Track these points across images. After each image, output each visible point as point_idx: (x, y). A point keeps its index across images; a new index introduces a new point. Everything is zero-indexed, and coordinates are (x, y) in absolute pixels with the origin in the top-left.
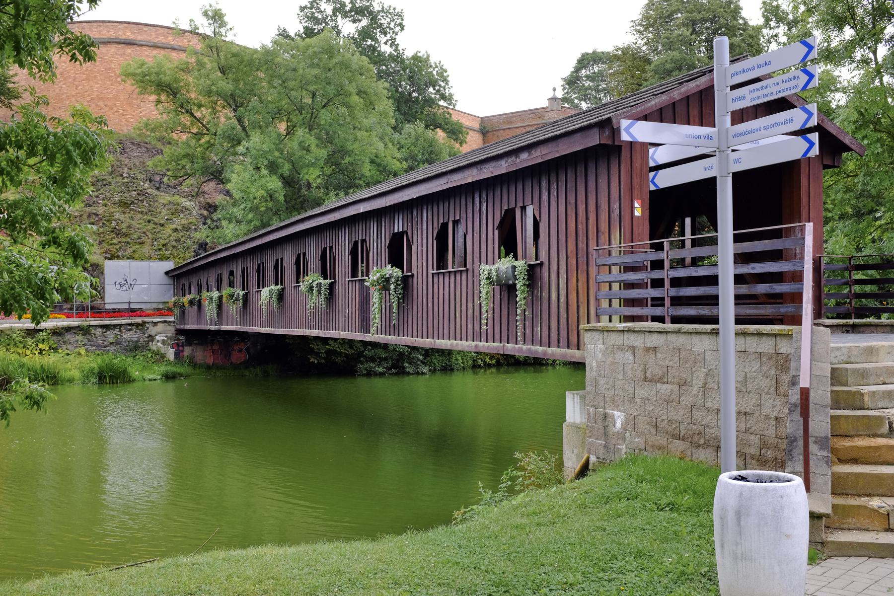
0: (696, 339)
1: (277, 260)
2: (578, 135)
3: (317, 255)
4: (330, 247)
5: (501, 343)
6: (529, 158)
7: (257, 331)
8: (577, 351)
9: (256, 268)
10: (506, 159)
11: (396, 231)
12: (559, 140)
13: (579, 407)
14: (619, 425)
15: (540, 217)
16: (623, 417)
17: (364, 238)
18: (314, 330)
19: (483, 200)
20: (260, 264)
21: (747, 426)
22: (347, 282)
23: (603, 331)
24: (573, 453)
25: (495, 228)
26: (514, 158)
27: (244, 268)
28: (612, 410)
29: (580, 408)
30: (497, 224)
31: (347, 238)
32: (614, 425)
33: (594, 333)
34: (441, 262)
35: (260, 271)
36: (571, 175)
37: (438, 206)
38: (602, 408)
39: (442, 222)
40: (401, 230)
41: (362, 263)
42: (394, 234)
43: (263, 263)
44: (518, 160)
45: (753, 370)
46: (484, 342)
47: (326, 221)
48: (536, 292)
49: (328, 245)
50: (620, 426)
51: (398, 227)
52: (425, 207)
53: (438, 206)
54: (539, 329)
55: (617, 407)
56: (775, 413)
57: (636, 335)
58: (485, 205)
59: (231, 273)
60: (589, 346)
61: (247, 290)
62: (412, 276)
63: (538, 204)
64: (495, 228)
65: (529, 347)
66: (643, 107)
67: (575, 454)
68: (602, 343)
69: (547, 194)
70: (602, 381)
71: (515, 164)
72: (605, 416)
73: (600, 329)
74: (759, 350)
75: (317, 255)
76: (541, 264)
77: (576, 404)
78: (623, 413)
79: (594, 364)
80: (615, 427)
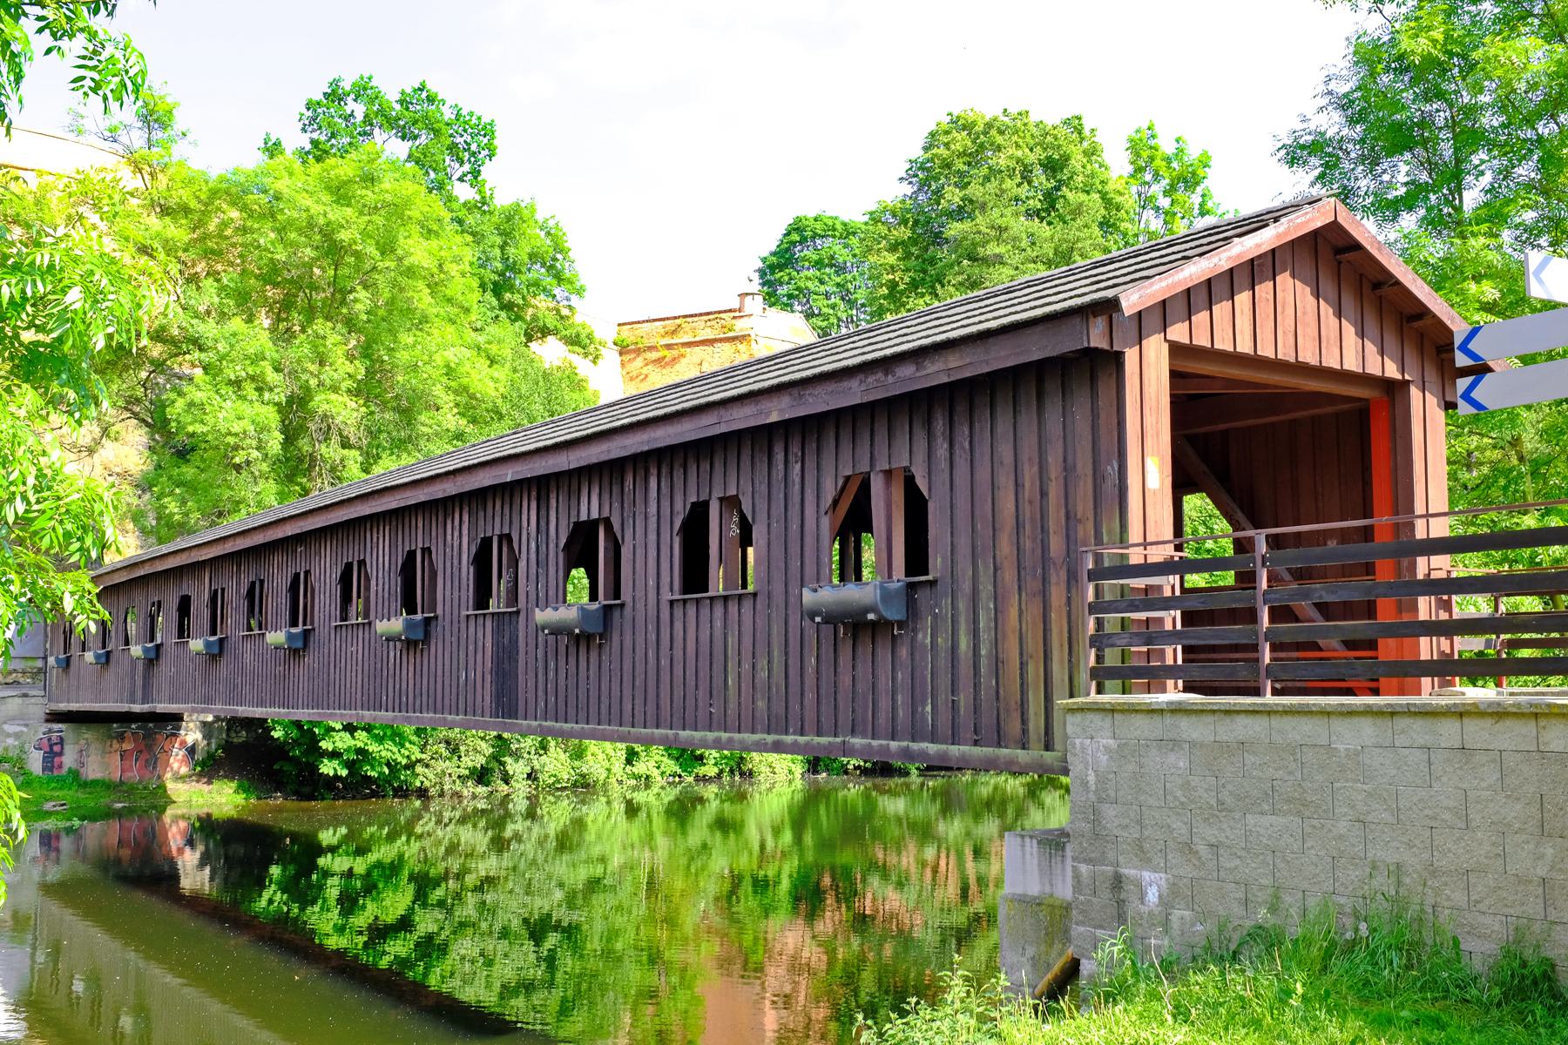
0: (1339, 725)
1: (297, 576)
2: (1039, 328)
3: (393, 567)
4: (423, 549)
5: (835, 736)
6: (918, 374)
7: (245, 715)
8: (1019, 751)
9: (244, 590)
10: (862, 376)
11: (584, 517)
12: (991, 340)
13: (1035, 862)
14: (1152, 896)
15: (930, 489)
16: (1163, 883)
17: (506, 531)
18: (383, 713)
19: (792, 458)
20: (253, 584)
21: (1472, 898)
22: (463, 620)
23: (1112, 710)
24: (1023, 955)
25: (822, 511)
26: (880, 375)
27: (216, 591)
28: (1135, 868)
29: (1039, 865)
30: (562, 545)
31: (465, 532)
32: (1142, 898)
33: (1090, 716)
34: (694, 576)
35: (254, 598)
36: (706, 466)
37: (685, 473)
38: (1112, 865)
39: (694, 499)
40: (595, 515)
41: (359, 597)
42: (578, 525)
43: (262, 582)
44: (890, 379)
45: (1484, 785)
46: (762, 732)
47: (423, 498)
48: (920, 636)
49: (420, 545)
50: (1156, 900)
51: (590, 507)
52: (654, 471)
53: (685, 473)
54: (929, 708)
55: (1146, 862)
56: (1541, 871)
57: (1194, 718)
58: (798, 467)
59: (184, 606)
60: (1078, 741)
61: (222, 633)
62: (436, 618)
63: (926, 465)
64: (822, 511)
65: (905, 744)
66: (1170, 281)
67: (1028, 956)
68: (1110, 734)
69: (946, 446)
70: (1109, 812)
71: (444, 491)
72: (1118, 882)
73: (1108, 707)
74: (1496, 745)
75: (393, 567)
76: (622, 605)
77: (1028, 856)
78: (1163, 875)
79: (1089, 778)
80: (1143, 903)
